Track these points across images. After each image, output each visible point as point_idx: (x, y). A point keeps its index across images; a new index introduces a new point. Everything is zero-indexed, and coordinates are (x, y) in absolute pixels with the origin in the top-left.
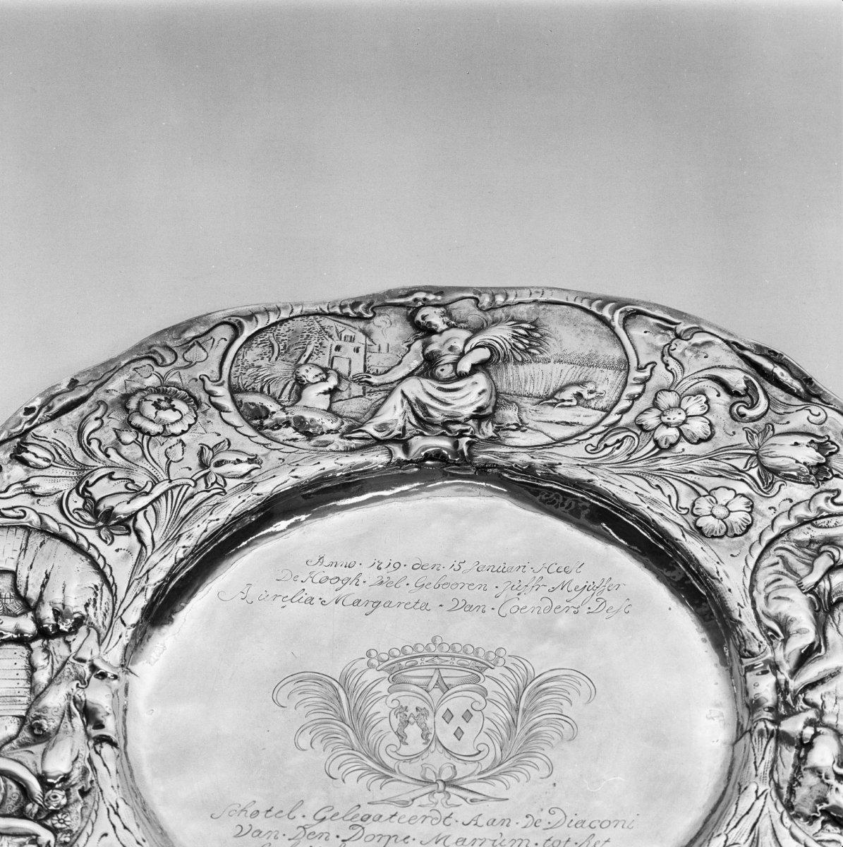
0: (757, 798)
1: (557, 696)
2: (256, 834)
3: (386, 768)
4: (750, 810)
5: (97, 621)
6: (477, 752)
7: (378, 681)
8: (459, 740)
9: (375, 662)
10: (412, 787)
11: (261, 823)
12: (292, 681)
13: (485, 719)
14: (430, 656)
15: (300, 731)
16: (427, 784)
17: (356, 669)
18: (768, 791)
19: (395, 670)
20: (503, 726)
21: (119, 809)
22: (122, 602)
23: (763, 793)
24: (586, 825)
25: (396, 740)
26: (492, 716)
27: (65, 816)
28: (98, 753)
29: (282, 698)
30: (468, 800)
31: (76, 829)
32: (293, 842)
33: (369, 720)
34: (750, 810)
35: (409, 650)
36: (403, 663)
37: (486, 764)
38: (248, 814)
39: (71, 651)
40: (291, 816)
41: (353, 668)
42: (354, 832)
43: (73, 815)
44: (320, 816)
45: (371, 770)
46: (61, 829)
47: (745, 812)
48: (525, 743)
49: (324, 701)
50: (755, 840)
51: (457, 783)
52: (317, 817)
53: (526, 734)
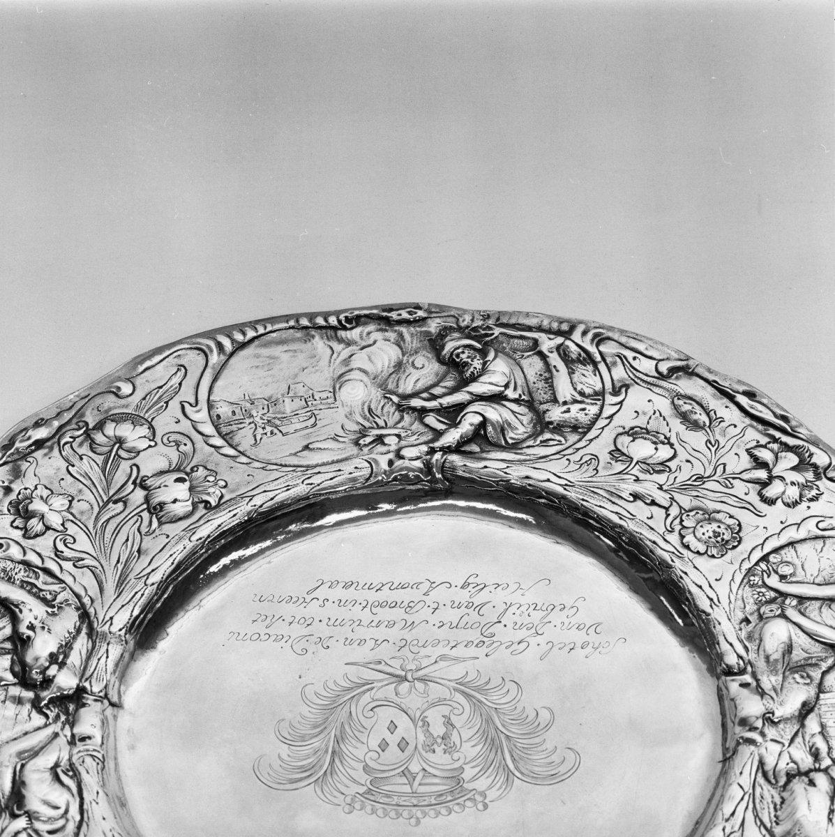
0: (111, 618)
1: (293, 764)
2: (582, 627)
3: (463, 692)
4: (120, 609)
5: (769, 791)
6: (375, 710)
7: (475, 778)
8: (392, 721)
9: (479, 798)
10: (437, 674)
11: (579, 637)
12: (562, 775)
13: (365, 742)
14: (422, 806)
15: (549, 726)
16: (423, 678)
17: (498, 790)
18: (99, 626)
19: (458, 791)
20: (348, 736)
21: (709, 604)
22: (747, 808)
23: (106, 623)
24: (273, 638)
25: (454, 719)
26: (359, 745)
27: (759, 599)
28: (740, 657)
29: (571, 756)
30: (383, 663)
31: (746, 588)
32: (546, 620)
33: (481, 739)
34: (120, 609)
35: (444, 811)
36: (449, 798)
37: (366, 698)
38: (591, 645)
39: (789, 752)
40: (551, 644)
41: (501, 790)
42: (490, 630)
43: (752, 601)
44: (524, 645)
45: (478, 689)
46: (759, 587)
47: (125, 607)
48: (328, 718)
49: (530, 757)
50: (119, 585)
51: (394, 679)
52: (526, 644)
53: (325, 728)
